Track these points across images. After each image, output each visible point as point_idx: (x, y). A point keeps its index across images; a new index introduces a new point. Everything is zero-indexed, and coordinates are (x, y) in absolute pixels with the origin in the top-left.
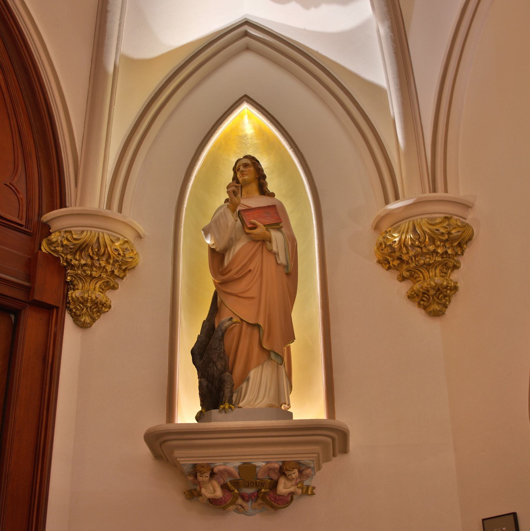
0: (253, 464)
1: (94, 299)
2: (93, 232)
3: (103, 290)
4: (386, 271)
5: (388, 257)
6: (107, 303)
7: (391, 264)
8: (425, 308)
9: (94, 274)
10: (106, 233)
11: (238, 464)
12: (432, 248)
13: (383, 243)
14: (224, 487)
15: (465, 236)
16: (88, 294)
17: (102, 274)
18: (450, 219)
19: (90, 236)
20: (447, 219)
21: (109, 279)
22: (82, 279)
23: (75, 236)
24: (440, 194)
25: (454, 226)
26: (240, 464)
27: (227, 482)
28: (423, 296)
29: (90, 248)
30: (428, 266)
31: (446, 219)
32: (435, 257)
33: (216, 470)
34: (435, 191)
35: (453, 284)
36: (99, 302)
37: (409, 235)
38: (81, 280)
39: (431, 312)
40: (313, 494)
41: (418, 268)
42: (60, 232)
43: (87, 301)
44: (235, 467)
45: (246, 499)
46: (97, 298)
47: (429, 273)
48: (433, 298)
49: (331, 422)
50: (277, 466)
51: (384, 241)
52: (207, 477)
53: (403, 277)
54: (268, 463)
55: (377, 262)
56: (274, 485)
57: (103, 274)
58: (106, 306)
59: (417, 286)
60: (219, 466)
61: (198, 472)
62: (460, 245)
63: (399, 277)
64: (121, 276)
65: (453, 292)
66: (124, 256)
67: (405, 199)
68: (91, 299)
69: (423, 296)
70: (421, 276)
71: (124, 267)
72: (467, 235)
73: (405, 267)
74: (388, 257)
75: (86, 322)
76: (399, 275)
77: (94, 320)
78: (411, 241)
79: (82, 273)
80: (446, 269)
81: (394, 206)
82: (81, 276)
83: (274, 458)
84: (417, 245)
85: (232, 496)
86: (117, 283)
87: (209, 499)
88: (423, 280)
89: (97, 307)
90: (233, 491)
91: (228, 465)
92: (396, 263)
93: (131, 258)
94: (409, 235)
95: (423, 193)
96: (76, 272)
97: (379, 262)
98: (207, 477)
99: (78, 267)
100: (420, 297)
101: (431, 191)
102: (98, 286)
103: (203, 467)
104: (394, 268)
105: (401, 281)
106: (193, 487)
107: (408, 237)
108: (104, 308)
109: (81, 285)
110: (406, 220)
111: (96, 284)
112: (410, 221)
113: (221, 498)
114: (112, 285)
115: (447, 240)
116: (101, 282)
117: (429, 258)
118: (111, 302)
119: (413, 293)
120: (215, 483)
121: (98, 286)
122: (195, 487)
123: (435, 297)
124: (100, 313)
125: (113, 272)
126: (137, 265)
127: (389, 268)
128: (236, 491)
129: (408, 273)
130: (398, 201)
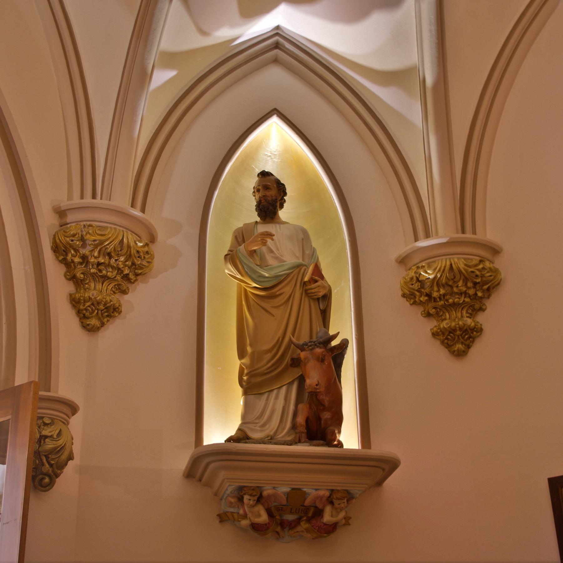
0: (305, 490)
1: (109, 301)
7: (417, 300)
11: (286, 489)
12: (464, 289)
24: (468, 235)
27: (271, 507)
28: (448, 335)
32: (464, 298)
33: (265, 493)
34: (463, 232)
39: (454, 351)
44: (284, 493)
48: (459, 338)
49: (367, 452)
51: (416, 277)
52: (255, 500)
54: (316, 490)
56: (319, 513)
59: (444, 324)
65: (479, 334)
67: (442, 237)
69: (448, 335)
73: (431, 305)
77: (469, 347)
79: (445, 302)
80: (472, 311)
85: (274, 522)
91: (277, 489)
92: (424, 299)
97: (404, 296)
100: (446, 335)
102: (110, 287)
116: (114, 284)
119: (439, 331)
121: (110, 287)
123: (460, 337)
127: (415, 303)
129: (434, 310)
130: (429, 239)
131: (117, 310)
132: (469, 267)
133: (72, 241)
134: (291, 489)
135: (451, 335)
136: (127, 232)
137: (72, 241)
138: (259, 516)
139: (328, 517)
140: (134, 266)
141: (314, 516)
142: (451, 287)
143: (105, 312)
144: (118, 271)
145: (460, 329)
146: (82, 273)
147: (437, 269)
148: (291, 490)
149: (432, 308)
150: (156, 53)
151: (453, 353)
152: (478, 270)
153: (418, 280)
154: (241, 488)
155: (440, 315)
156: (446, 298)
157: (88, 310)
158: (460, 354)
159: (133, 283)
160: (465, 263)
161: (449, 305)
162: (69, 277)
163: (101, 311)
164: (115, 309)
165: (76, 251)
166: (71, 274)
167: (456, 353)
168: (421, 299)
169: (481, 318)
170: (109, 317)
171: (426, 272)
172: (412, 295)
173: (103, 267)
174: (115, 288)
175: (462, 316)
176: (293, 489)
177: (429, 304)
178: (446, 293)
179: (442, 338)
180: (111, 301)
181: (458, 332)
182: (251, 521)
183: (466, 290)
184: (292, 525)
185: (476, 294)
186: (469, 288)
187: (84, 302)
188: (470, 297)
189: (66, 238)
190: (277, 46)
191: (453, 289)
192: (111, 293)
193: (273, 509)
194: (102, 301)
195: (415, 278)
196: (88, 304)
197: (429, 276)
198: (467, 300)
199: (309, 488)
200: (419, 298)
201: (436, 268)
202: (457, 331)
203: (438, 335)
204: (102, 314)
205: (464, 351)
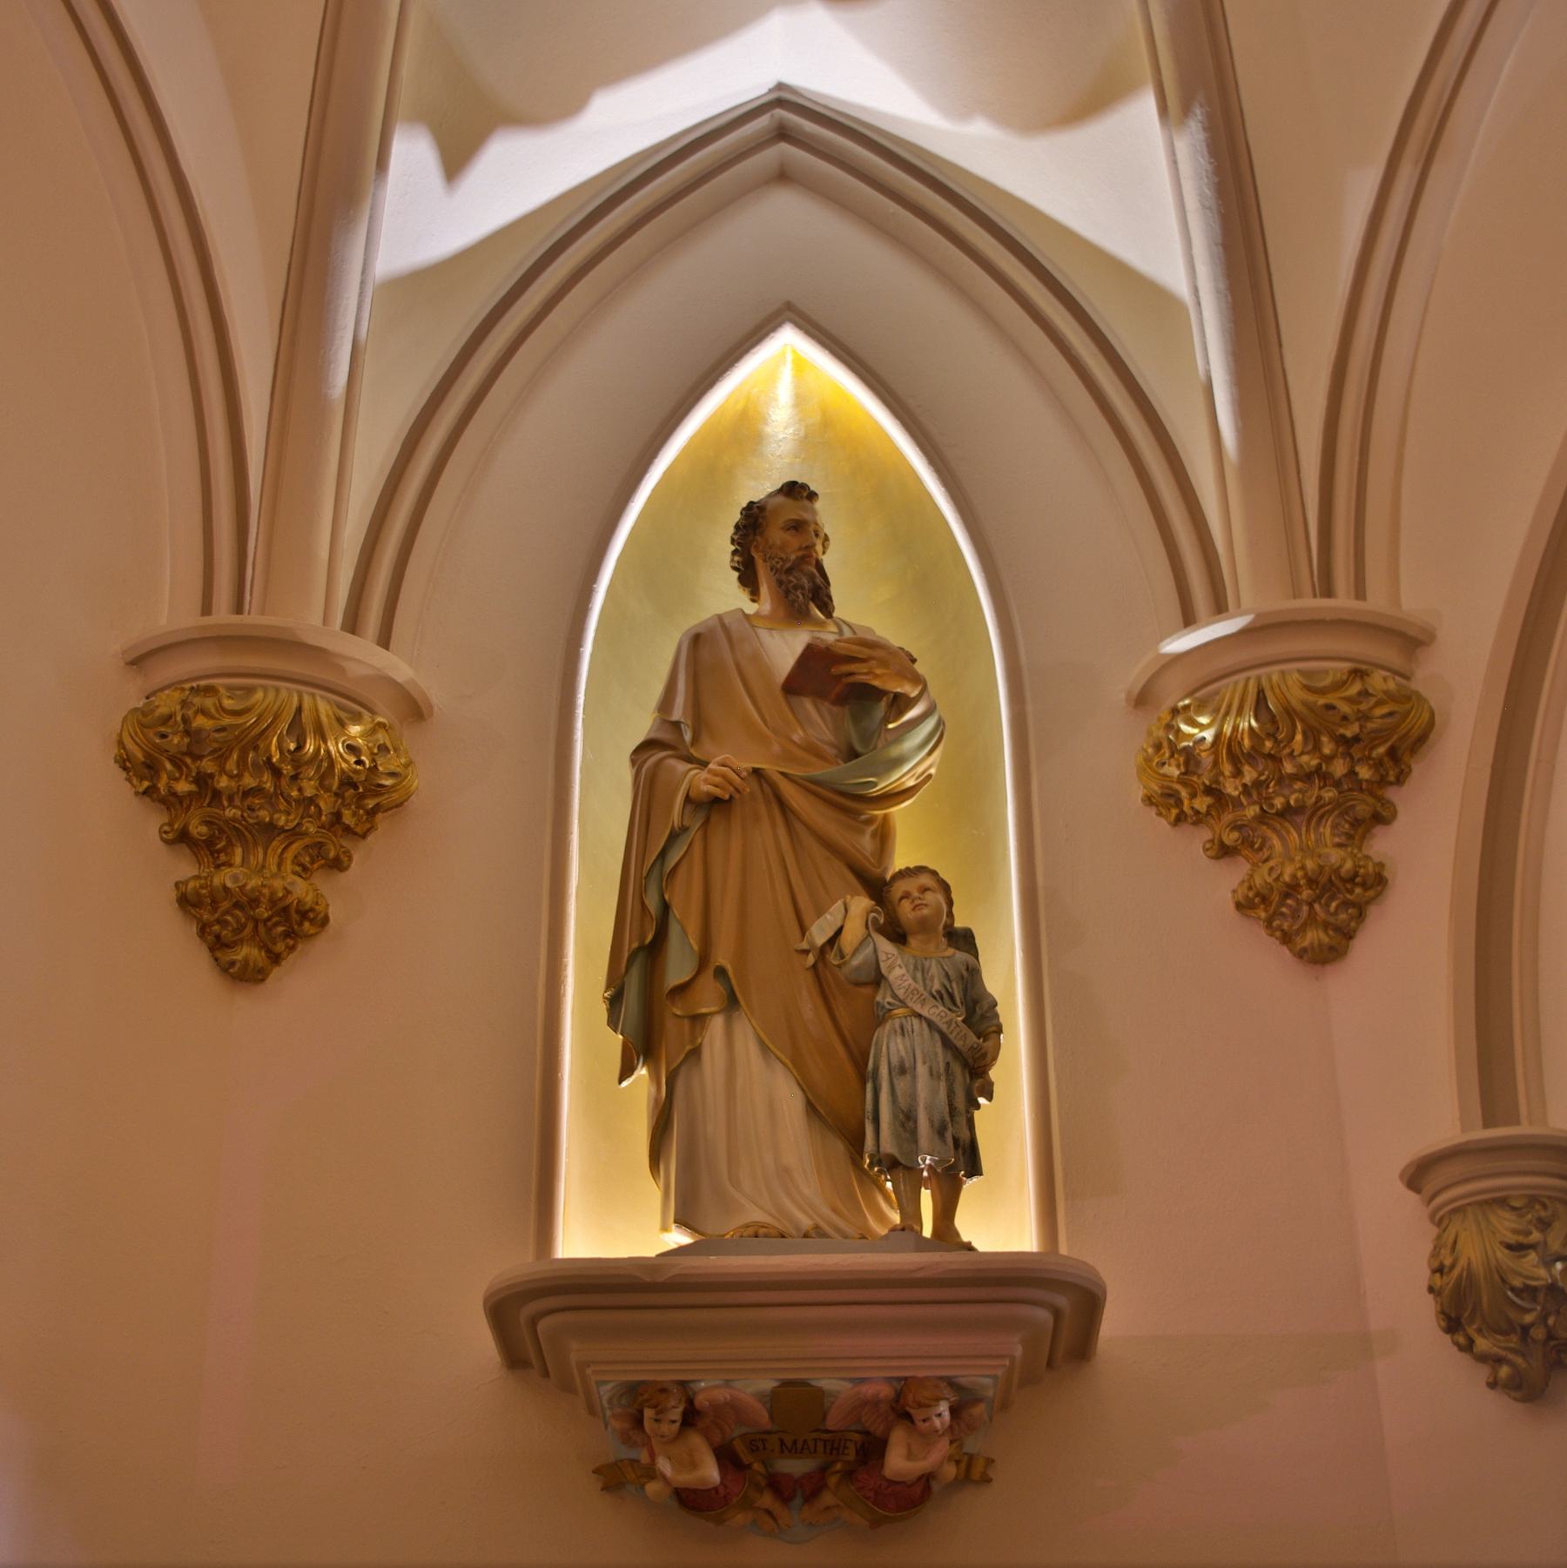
2: (284, 694)
3: (305, 869)
5: (1178, 787)
6: (317, 907)
8: (1286, 939)
9: (282, 820)
10: (322, 697)
11: (767, 1384)
12: (1310, 761)
13: (1165, 744)
14: (726, 1456)
15: (1410, 726)
16: (262, 879)
18: (1368, 675)
19: (275, 703)
20: (1359, 674)
21: (327, 838)
22: (243, 833)
23: (228, 703)
24: (1343, 601)
25: (1379, 697)
26: (773, 1384)
27: (733, 1439)
30: (271, 829)
31: (1356, 675)
32: (1320, 788)
33: (701, 1401)
34: (1328, 592)
35: (1371, 869)
36: (295, 902)
37: (1247, 719)
40: (986, 1480)
44: (760, 1396)
48: (256, 927)
50: (886, 1391)
52: (674, 1422)
55: (1143, 800)
56: (873, 1449)
57: (309, 822)
58: (315, 918)
59: (1262, 877)
60: (709, 1389)
61: (648, 1407)
62: (1393, 753)
63: (1208, 846)
64: (358, 830)
65: (1371, 893)
66: (374, 769)
68: (273, 894)
71: (370, 803)
72: (1415, 724)
74: (1178, 787)
75: (252, 964)
76: (1209, 841)
78: (1251, 738)
82: (240, 824)
83: (879, 1368)
85: (747, 1484)
86: (349, 852)
87: (676, 1489)
89: (288, 919)
90: (749, 1466)
92: (1202, 803)
93: (393, 774)
94: (1247, 719)
101: (1318, 594)
102: (289, 855)
103: (663, 1390)
104: (1194, 818)
105: (1217, 858)
106: (625, 1453)
107: (1244, 725)
108: (307, 924)
110: (1235, 678)
111: (284, 849)
112: (1248, 679)
113: (716, 1489)
114: (332, 854)
115: (1356, 739)
118: (328, 905)
120: (696, 1441)
121: (289, 855)
122: (633, 1454)
125: (338, 816)
126: (409, 797)
127: (1180, 819)
128: (757, 1466)
131: (311, 915)
132: (1322, 692)
133: (164, 736)
135: (238, 913)
136: (313, 695)
137: (164, 736)
139: (899, 1462)
142: (1274, 758)
143: (276, 924)
148: (779, 1386)
149: (1227, 830)
151: (1301, 954)
152: (1349, 700)
153: (1174, 750)
155: (219, 847)
157: (226, 923)
158: (247, 977)
159: (364, 836)
160: (1304, 682)
162: (170, 836)
163: (265, 924)
164: (304, 914)
166: (176, 826)
167: (236, 968)
169: (1382, 845)
170: (292, 938)
171: (1194, 724)
172: (1170, 795)
173: (262, 801)
178: (1263, 778)
183: (1320, 764)
184: (812, 1488)
185: (1352, 773)
186: (1329, 759)
188: (1337, 784)
189: (145, 730)
190: (783, 133)
191: (1283, 766)
193: (739, 1447)
195: (1165, 744)
197: (1201, 731)
198: (1329, 794)
199: (834, 1378)
200: (1191, 803)
202: (258, 907)
205: (1331, 948)
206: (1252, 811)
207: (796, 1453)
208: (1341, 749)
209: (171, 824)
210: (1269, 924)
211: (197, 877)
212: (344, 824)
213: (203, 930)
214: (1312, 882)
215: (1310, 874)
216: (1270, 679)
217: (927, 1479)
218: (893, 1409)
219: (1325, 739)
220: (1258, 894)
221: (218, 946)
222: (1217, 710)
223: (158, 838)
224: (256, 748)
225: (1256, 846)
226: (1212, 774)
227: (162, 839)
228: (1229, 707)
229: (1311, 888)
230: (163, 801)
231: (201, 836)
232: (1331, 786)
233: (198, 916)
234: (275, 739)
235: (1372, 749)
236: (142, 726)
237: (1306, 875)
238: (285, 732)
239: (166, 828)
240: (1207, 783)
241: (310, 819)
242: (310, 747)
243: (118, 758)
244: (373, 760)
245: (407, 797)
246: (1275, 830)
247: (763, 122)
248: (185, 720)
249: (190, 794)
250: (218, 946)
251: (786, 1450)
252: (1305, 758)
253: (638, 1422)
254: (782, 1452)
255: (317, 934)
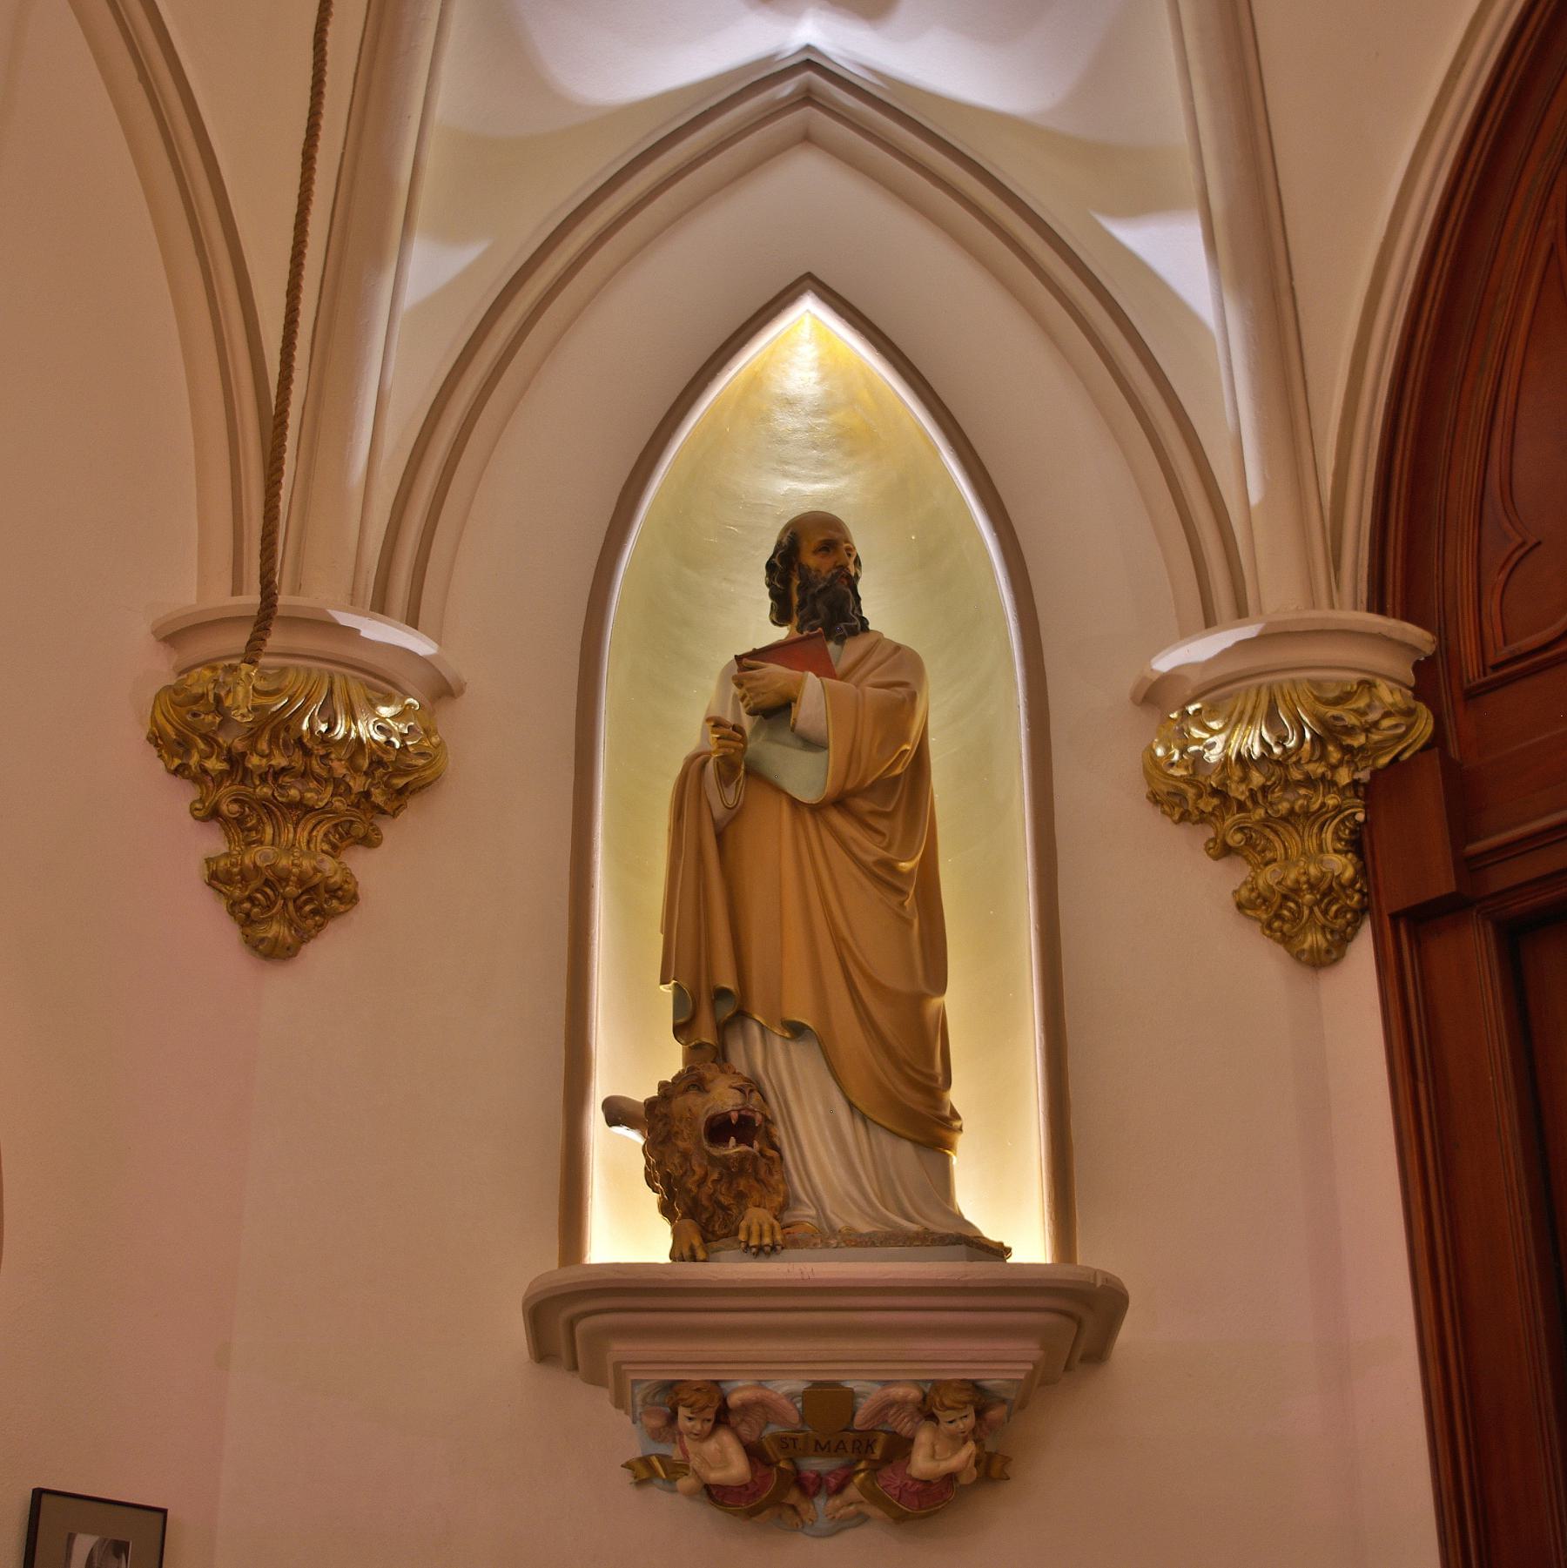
0: (849, 1385)
2: (315, 676)
4: (1175, 826)
6: (346, 886)
11: (797, 1385)
14: (754, 1452)
16: (292, 858)
17: (335, 799)
28: (1281, 907)
29: (308, 716)
30: (302, 809)
32: (1324, 796)
33: (734, 1400)
38: (270, 813)
41: (268, 808)
42: (214, 669)
43: (287, 880)
44: (790, 1396)
45: (811, 1489)
46: (316, 870)
47: (1303, 841)
48: (285, 904)
50: (914, 1394)
52: (709, 1420)
53: (1225, 844)
54: (886, 1383)
56: (901, 1447)
57: (339, 801)
61: (684, 1406)
64: (390, 811)
70: (1277, 845)
71: (400, 782)
73: (228, 789)
77: (304, 937)
81: (378, 631)
83: (904, 1371)
84: (1275, 758)
88: (1283, 857)
91: (770, 1386)
92: (1211, 803)
95: (1337, 605)
96: (257, 790)
98: (709, 1420)
99: (264, 776)
105: (1216, 858)
109: (269, 831)
115: (1362, 748)
117: (1306, 796)
123: (291, 906)
124: (323, 916)
125: (367, 794)
127: (1184, 817)
130: (1215, 628)
134: (810, 1385)
137: (195, 715)
138: (725, 1463)
139: (922, 1463)
140: (381, 769)
141: (887, 1459)
144: (336, 787)
145: (301, 881)
146: (235, 801)
147: (1236, 715)
150: (413, 167)
151: (1297, 956)
154: (670, 1387)
155: (249, 825)
156: (1269, 798)
159: (394, 816)
161: (1279, 818)
163: (294, 902)
164: (333, 892)
165: (209, 740)
166: (207, 804)
168: (1201, 805)
170: (321, 915)
171: (1206, 729)
174: (336, 831)
175: (1321, 849)
176: (816, 1384)
177: (1226, 817)
178: (1269, 783)
179: (1264, 916)
180: (316, 870)
181: (291, 890)
182: (699, 1477)
186: (1334, 768)
187: (244, 878)
190: (807, 97)
192: (323, 851)
194: (290, 872)
196: (254, 884)
197: (1212, 736)
201: (1232, 713)
202: (287, 885)
203: (1254, 907)
204: (299, 909)
206: (1260, 813)
207: (829, 1451)
208: (1346, 758)
209: (201, 800)
210: (1268, 926)
211: (228, 855)
212: (373, 802)
213: (233, 907)
214: (1312, 887)
215: (1312, 880)
216: (1281, 688)
217: (951, 1477)
218: (919, 1409)
219: (1331, 748)
220: (1259, 895)
221: (248, 923)
222: (1230, 717)
223: (191, 819)
224: (287, 729)
225: (1259, 848)
226: (1218, 778)
227: (196, 818)
228: (1242, 713)
229: (1311, 893)
230: (195, 780)
231: (231, 813)
232: (1334, 793)
233: (229, 894)
234: (307, 719)
235: (1375, 759)
236: (174, 703)
237: (1308, 882)
238: (316, 714)
239: (198, 806)
240: (1214, 785)
241: (339, 798)
242: (340, 731)
243: (151, 736)
244: (403, 742)
245: (437, 776)
246: (1276, 832)
247: (786, 89)
248: (218, 699)
249: (221, 772)
250: (248, 923)
251: (819, 1450)
252: (1310, 767)
253: (672, 1418)
254: (816, 1450)
255: (347, 911)
